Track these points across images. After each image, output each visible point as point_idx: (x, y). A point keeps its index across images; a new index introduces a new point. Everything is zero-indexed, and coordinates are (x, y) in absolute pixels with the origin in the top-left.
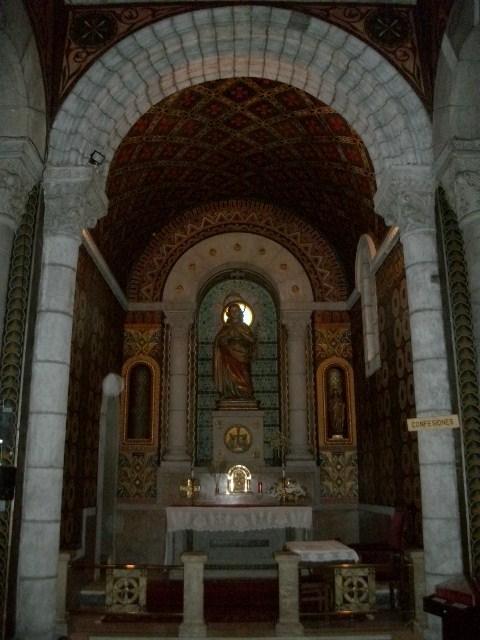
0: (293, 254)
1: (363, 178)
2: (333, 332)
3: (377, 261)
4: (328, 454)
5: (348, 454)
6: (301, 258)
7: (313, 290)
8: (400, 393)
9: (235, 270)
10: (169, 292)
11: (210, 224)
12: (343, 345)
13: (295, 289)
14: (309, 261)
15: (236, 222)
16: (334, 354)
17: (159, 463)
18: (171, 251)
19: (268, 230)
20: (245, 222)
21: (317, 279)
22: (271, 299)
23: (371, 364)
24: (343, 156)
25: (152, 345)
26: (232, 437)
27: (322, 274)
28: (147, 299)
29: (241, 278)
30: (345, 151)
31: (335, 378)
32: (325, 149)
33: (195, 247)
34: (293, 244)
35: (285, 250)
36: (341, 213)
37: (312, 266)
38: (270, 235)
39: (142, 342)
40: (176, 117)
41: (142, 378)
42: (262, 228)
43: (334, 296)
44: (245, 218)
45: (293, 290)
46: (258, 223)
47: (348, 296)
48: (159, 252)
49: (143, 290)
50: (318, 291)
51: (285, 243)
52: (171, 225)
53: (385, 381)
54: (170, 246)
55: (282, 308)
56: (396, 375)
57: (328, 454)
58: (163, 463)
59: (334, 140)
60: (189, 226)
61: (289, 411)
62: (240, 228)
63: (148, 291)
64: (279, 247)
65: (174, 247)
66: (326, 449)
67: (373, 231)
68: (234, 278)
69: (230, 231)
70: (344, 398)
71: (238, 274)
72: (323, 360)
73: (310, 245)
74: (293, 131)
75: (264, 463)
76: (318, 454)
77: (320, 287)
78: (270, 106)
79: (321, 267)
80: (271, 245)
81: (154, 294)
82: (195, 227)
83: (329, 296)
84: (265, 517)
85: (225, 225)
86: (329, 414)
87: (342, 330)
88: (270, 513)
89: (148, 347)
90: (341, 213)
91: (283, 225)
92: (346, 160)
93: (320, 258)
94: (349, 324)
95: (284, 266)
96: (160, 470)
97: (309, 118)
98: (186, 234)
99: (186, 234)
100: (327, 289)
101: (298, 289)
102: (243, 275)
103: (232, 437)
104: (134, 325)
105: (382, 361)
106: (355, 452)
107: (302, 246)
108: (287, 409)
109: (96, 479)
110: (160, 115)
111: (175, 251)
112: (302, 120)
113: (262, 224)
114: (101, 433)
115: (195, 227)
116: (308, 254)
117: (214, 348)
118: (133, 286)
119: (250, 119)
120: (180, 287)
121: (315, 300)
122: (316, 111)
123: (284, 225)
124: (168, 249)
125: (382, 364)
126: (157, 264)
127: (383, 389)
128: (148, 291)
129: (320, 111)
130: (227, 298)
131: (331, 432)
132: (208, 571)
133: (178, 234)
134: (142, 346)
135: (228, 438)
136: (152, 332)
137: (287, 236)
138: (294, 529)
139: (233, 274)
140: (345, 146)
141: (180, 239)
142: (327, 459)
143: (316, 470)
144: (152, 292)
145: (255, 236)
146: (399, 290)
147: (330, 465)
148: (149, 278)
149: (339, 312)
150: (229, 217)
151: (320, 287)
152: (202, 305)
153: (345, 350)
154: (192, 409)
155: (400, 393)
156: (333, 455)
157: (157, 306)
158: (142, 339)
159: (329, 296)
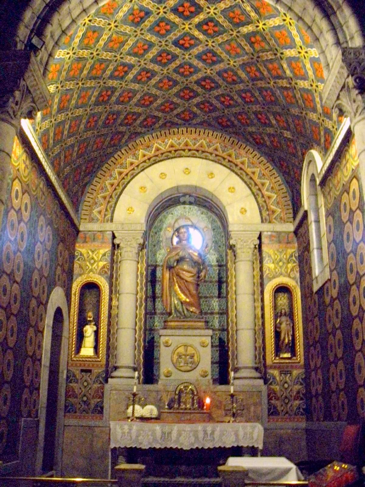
0: (241, 178)
1: (308, 91)
2: (281, 252)
3: (324, 172)
4: (276, 373)
5: (295, 372)
6: (250, 182)
7: (260, 212)
8: (351, 299)
9: (185, 195)
10: (120, 213)
11: (160, 149)
12: (290, 266)
13: (243, 211)
14: (256, 184)
15: (185, 148)
16: (281, 274)
17: (107, 381)
18: (123, 175)
19: (216, 155)
20: (195, 147)
21: (265, 202)
22: (219, 224)
23: (319, 279)
24: (288, 72)
25: (101, 264)
26: (180, 356)
27: (269, 198)
28: (98, 220)
29: (191, 203)
30: (290, 65)
31: (283, 300)
32: (270, 66)
33: (146, 171)
34: (241, 169)
35: (234, 175)
36: (287, 134)
37: (259, 190)
38: (218, 160)
39: (92, 261)
40: (125, 34)
41: (90, 298)
42: (211, 154)
43: (281, 218)
44: (195, 144)
45: (242, 213)
46: (207, 149)
47: (294, 218)
48: (111, 176)
49: (95, 211)
50: (265, 214)
51: (232, 166)
52: (123, 151)
53: (334, 293)
54: (122, 170)
55: (231, 228)
56: (347, 282)
57: (276, 373)
58: (109, 380)
59: (279, 55)
60: (141, 152)
61: (237, 330)
62: (190, 153)
63: (100, 212)
64: (227, 171)
65: (125, 171)
66: (274, 367)
67: (319, 144)
68: (184, 203)
69: (180, 156)
70: (291, 315)
71: (187, 199)
72: (270, 279)
73: (257, 170)
74: (239, 50)
75: (211, 381)
76: (265, 373)
77: (268, 209)
78: (217, 24)
79: (267, 190)
80: (221, 171)
81: (105, 215)
82: (147, 153)
83: (275, 219)
84: (213, 433)
85: (175, 151)
86: (277, 334)
87: (290, 251)
88: (218, 429)
89: (98, 266)
90: (287, 134)
91: (230, 151)
92: (291, 75)
93: (267, 182)
94: (296, 245)
95: (232, 189)
96: (107, 386)
97: (254, 34)
98: (137, 159)
99: (137, 159)
100: (273, 212)
101: (246, 211)
102: (192, 199)
103: (180, 356)
104: (85, 245)
105: (331, 271)
106: (304, 370)
107: (249, 170)
108: (235, 329)
109: (38, 389)
110: (130, 105)
111: (127, 175)
112: (248, 37)
113: (211, 150)
114: (61, 361)
115: (147, 153)
116: (256, 178)
117: (163, 270)
118: (85, 208)
119: (197, 39)
120: (130, 209)
121: (262, 222)
122: (261, 25)
123: (232, 152)
124: (120, 173)
125: (331, 275)
126: (109, 187)
127: (333, 300)
128: (100, 212)
129: (264, 24)
130: (176, 220)
131: (278, 350)
132: (36, 472)
133: (130, 159)
134: (92, 264)
135: (175, 357)
136: (102, 252)
137: (234, 161)
138: (242, 447)
139: (182, 200)
140: (290, 60)
141: (132, 164)
142: (274, 378)
143: (264, 388)
144: (103, 213)
145: (204, 161)
146: (348, 193)
147: (278, 384)
148: (102, 201)
149: (285, 232)
150: (179, 144)
151: (267, 209)
152: (153, 230)
153: (292, 270)
154: (140, 329)
155: (351, 299)
156: (281, 373)
157: (109, 227)
158: (93, 258)
159: (275, 219)
